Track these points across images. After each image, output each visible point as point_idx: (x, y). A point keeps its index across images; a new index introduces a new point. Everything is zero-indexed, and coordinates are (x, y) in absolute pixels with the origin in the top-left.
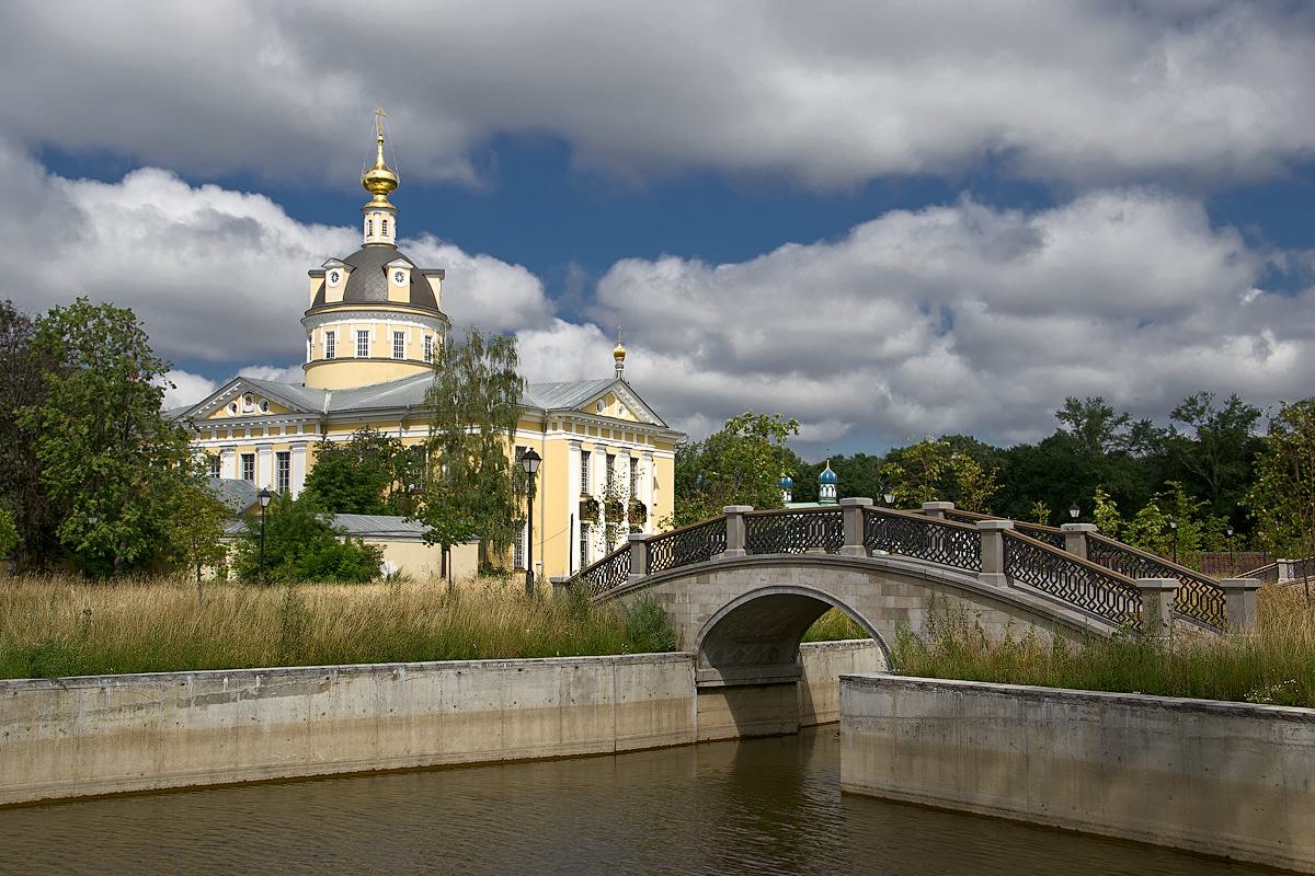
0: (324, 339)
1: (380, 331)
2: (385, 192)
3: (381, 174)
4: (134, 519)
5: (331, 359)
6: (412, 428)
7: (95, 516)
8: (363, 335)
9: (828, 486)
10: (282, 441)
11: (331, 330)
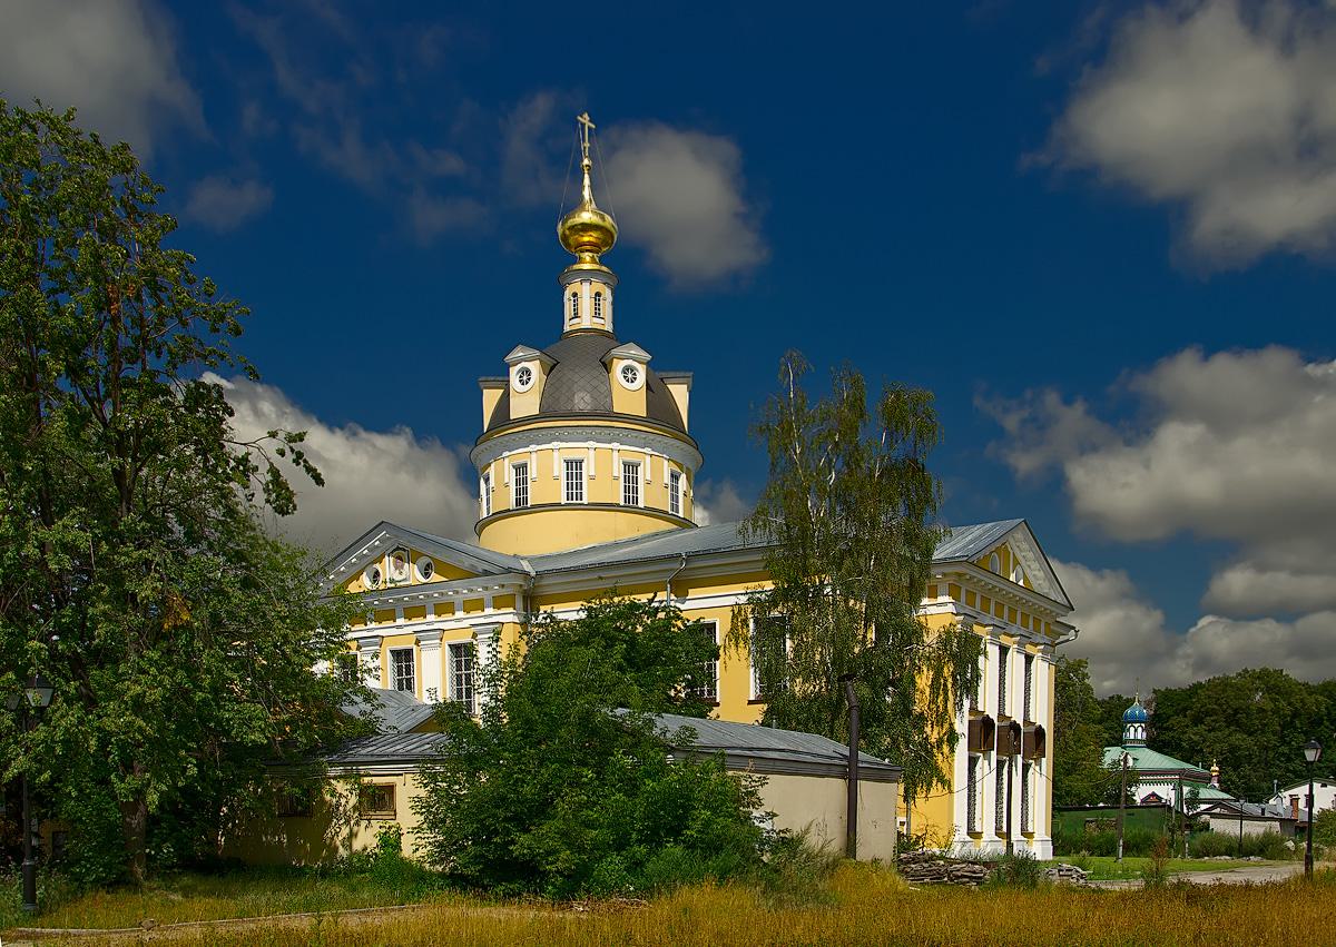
0: (510, 476)
1: (603, 462)
2: (594, 247)
3: (586, 216)
4: (155, 695)
5: (522, 507)
6: (692, 593)
7: (43, 683)
8: (574, 466)
9: (1136, 725)
10: (459, 626)
11: (521, 461)
